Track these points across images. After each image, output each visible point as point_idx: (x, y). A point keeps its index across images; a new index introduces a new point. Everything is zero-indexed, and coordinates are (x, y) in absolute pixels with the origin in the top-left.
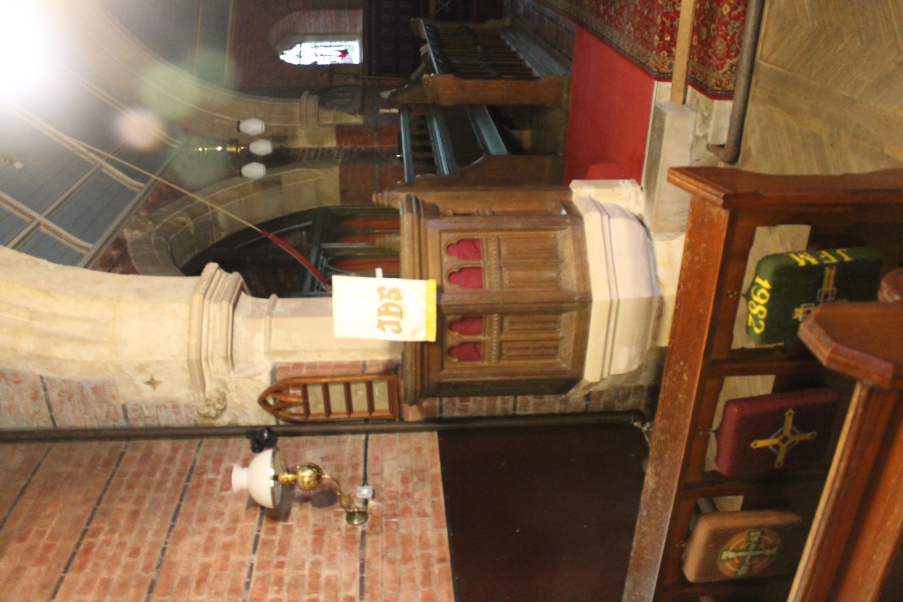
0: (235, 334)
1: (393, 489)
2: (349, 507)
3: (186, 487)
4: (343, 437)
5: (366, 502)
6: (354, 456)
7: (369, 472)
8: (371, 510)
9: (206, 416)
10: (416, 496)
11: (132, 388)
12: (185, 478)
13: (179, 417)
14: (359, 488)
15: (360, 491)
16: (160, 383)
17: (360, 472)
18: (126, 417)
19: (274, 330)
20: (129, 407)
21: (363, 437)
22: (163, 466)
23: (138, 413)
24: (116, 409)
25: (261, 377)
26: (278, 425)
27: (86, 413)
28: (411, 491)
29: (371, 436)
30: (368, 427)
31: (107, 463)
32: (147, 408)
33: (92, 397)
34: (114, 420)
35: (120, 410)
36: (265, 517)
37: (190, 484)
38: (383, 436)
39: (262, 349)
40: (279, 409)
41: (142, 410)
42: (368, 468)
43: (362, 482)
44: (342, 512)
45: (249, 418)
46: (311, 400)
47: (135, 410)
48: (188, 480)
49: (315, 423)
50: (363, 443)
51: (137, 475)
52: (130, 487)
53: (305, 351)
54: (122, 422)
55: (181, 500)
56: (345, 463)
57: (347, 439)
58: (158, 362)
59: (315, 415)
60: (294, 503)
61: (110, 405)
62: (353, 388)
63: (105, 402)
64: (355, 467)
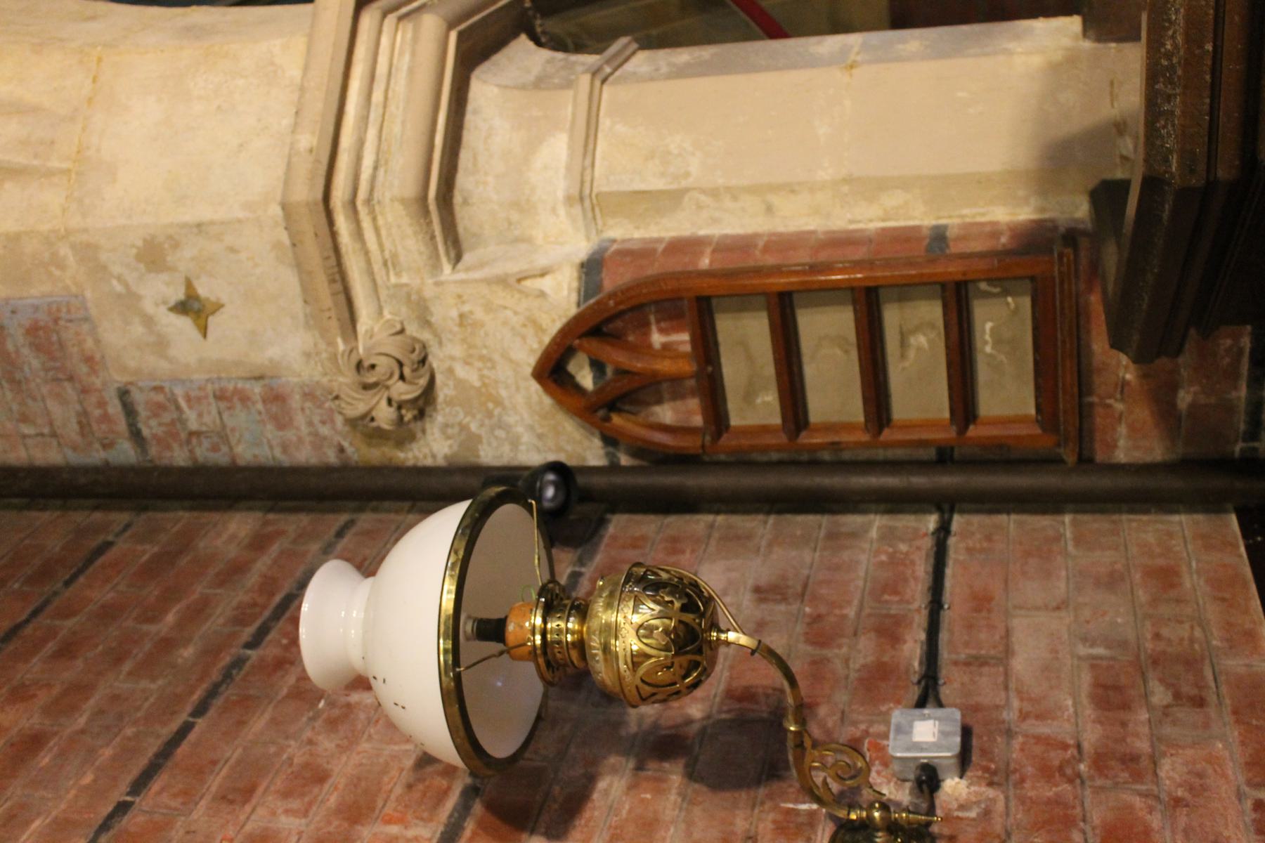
0: (470, 137)
1: (1059, 728)
2: (849, 799)
3: (239, 663)
4: (852, 521)
5: (928, 779)
6: (893, 586)
7: (945, 654)
8: (947, 819)
9: (362, 425)
10: (1171, 771)
11: (138, 330)
12: (248, 632)
13: (290, 435)
14: (897, 716)
15: (904, 730)
16: (218, 307)
17: (912, 649)
18: (136, 435)
19: (605, 123)
20: (138, 397)
21: (931, 522)
22: (199, 589)
23: (167, 417)
24: (102, 404)
25: (546, 284)
26: (614, 468)
27: (24, 419)
28: (1142, 745)
29: (957, 521)
30: (948, 480)
31: (44, 573)
32: (188, 399)
33: (32, 362)
34: (106, 446)
35: (115, 408)
36: (478, 808)
37: (253, 654)
38: (1010, 523)
39: (560, 186)
40: (613, 405)
41: (178, 408)
42: (944, 636)
43: (915, 693)
44: (811, 814)
45: (515, 443)
46: (732, 371)
47: (158, 409)
48: (254, 643)
49: (743, 462)
50: (928, 543)
51: (108, 613)
52: (67, 651)
53: (714, 193)
54: (125, 453)
55: (200, 710)
56: (851, 612)
57: (866, 529)
58: (199, 227)
59: (746, 431)
60: (613, 760)
61: (85, 391)
62: (892, 317)
63: (71, 379)
64: (889, 631)
